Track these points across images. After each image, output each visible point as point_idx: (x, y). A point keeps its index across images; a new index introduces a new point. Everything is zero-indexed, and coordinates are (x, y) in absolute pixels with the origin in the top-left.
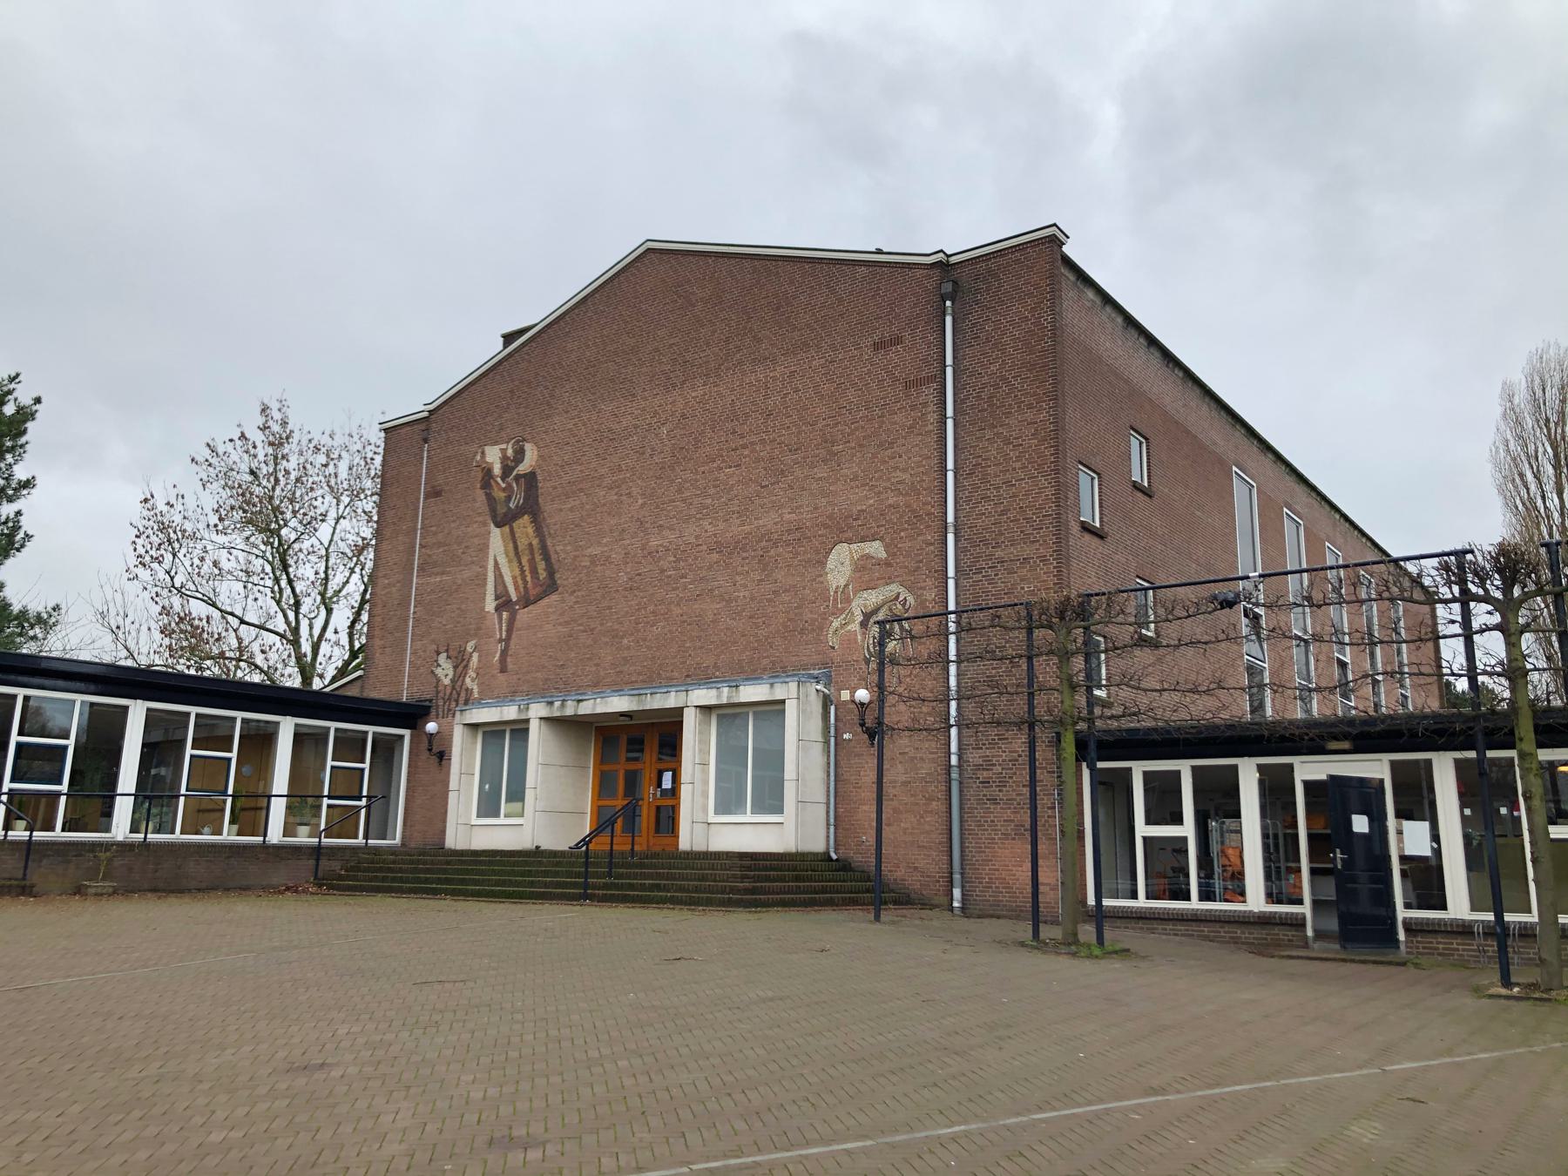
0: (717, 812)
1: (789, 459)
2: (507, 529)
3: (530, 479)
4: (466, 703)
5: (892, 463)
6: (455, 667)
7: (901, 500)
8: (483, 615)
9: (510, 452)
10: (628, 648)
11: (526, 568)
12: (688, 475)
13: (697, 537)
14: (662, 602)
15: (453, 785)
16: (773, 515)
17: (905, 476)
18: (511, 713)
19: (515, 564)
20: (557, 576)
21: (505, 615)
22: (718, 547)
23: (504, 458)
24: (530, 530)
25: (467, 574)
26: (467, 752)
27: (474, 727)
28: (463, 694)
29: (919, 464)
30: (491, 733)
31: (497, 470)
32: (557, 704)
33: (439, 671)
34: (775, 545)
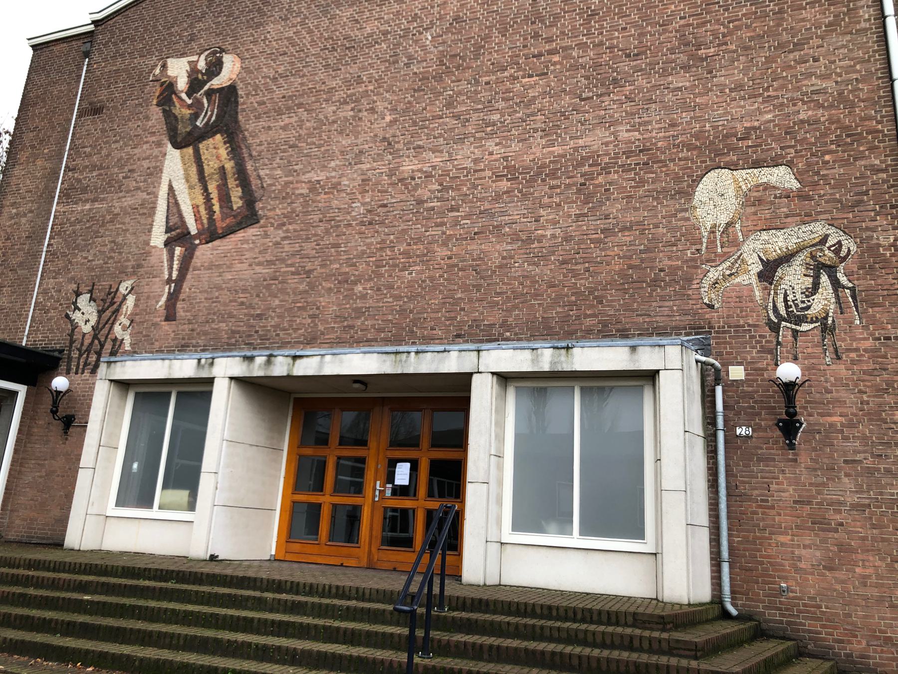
0: (517, 526)
1: (625, 66)
2: (190, 150)
3: (229, 94)
4: (113, 353)
5: (801, 68)
6: (100, 313)
7: (822, 115)
8: (146, 250)
9: (202, 65)
10: (364, 297)
11: (214, 195)
12: (463, 86)
13: (476, 161)
14: (418, 240)
15: (87, 458)
16: (602, 134)
17: (829, 85)
18: (184, 368)
19: (198, 190)
20: (259, 205)
21: (178, 251)
22: (511, 172)
23: (193, 71)
24: (223, 152)
25: (128, 201)
26: (108, 416)
27: (124, 385)
28: (108, 346)
29: (850, 69)
30: (149, 395)
31: (182, 84)
32: (260, 360)
33: (77, 316)
34: (606, 170)
